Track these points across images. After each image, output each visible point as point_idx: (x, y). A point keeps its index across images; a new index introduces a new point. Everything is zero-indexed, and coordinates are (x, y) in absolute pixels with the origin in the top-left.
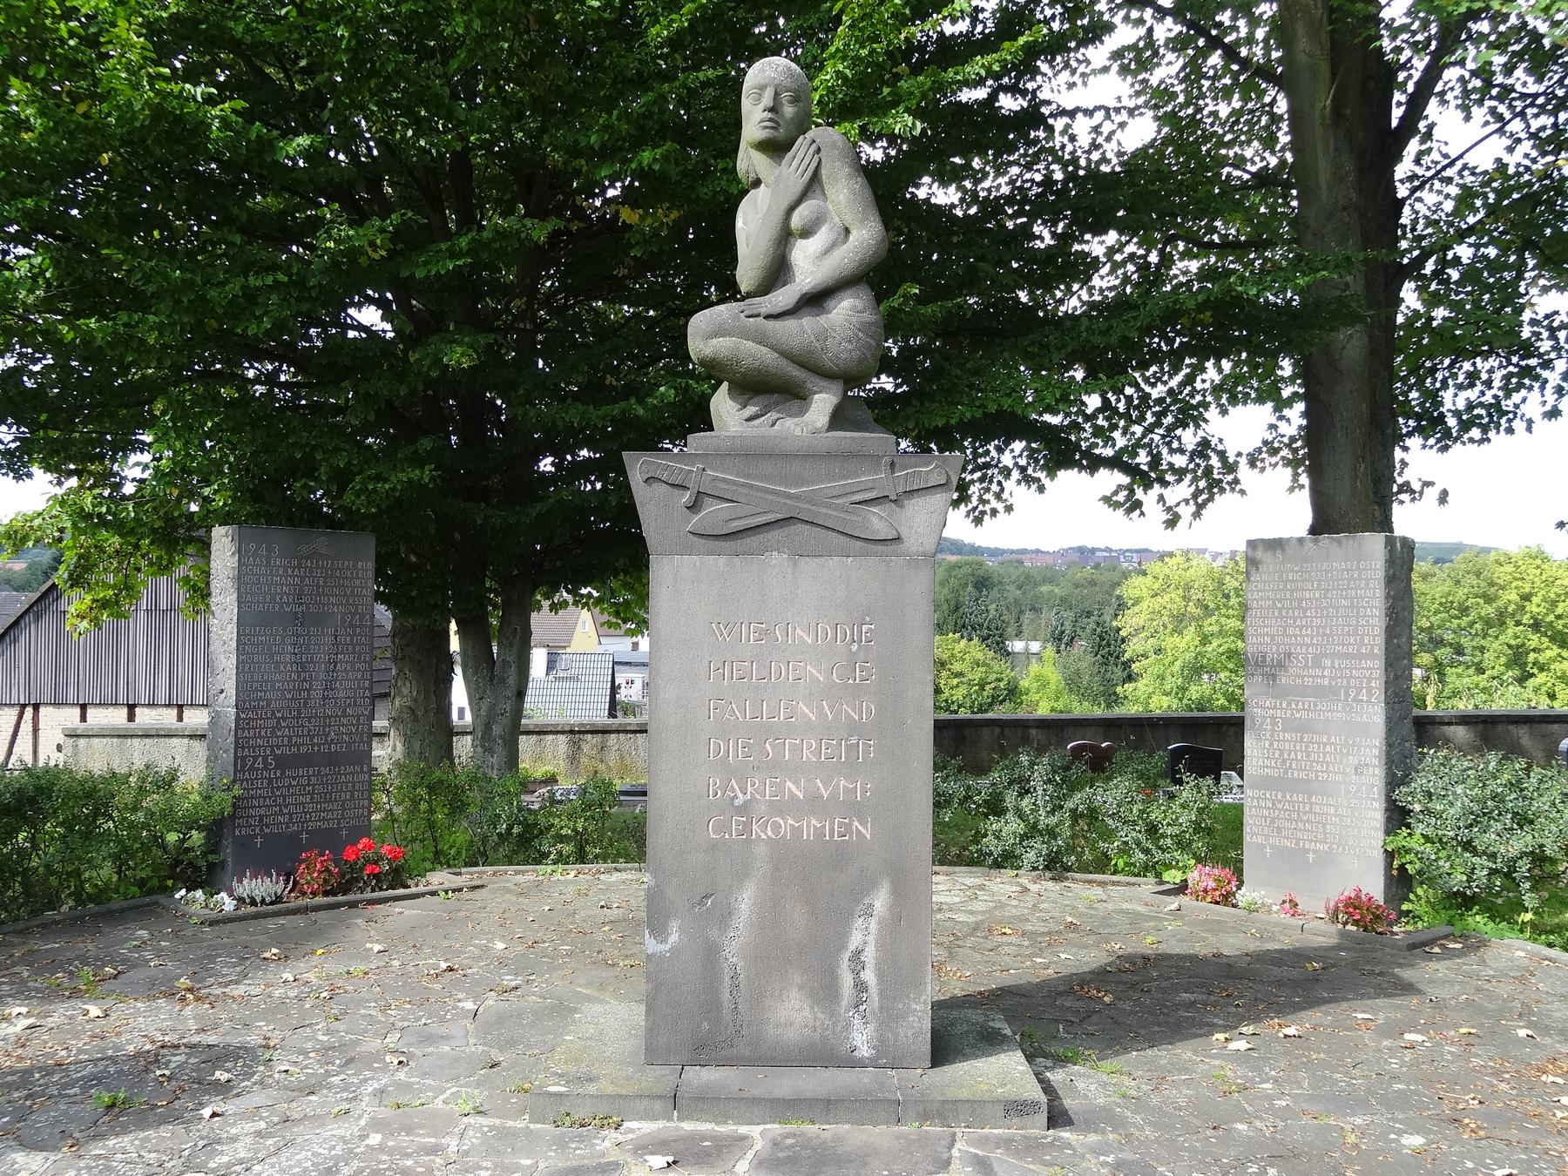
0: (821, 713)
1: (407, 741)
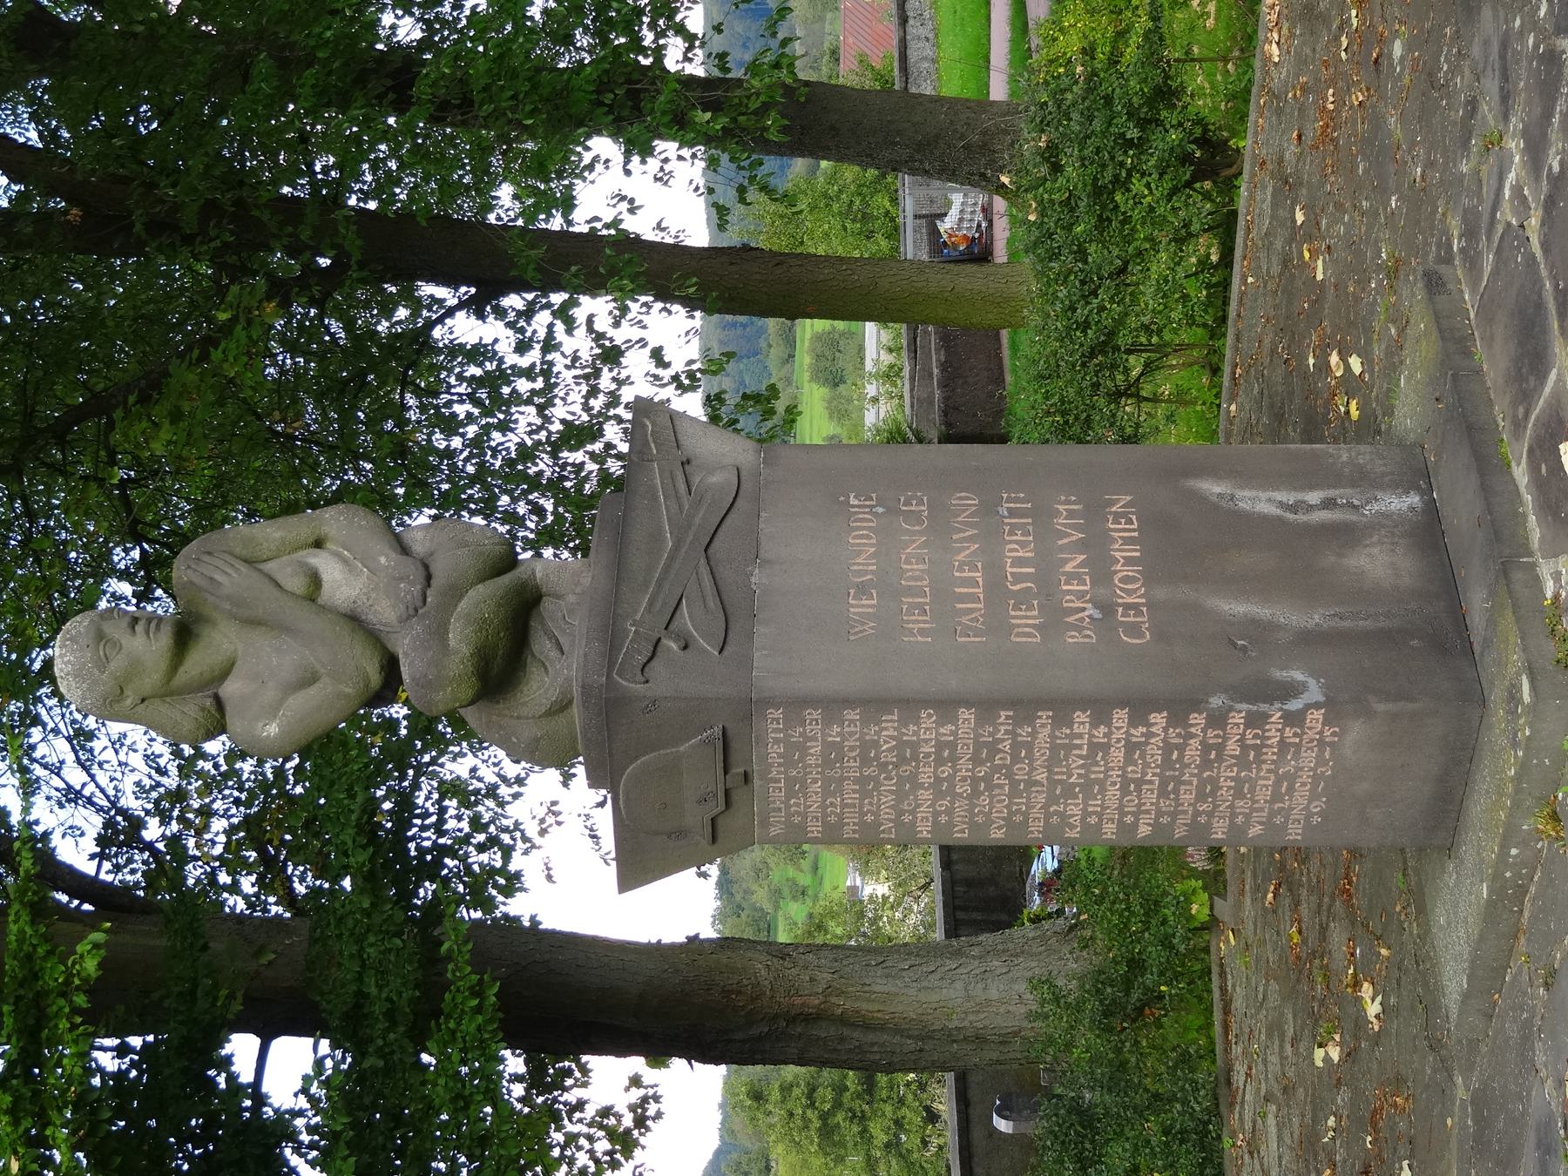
0: (971, 539)
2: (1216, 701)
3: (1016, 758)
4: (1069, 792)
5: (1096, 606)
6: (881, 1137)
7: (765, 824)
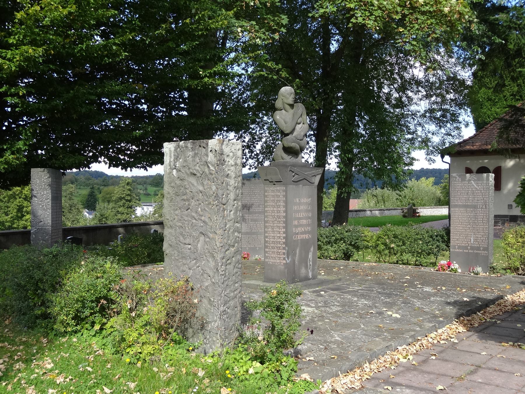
1: (370, 217)
2: (287, 248)
4: (272, 229)
6: (120, 210)
7: (267, 187)
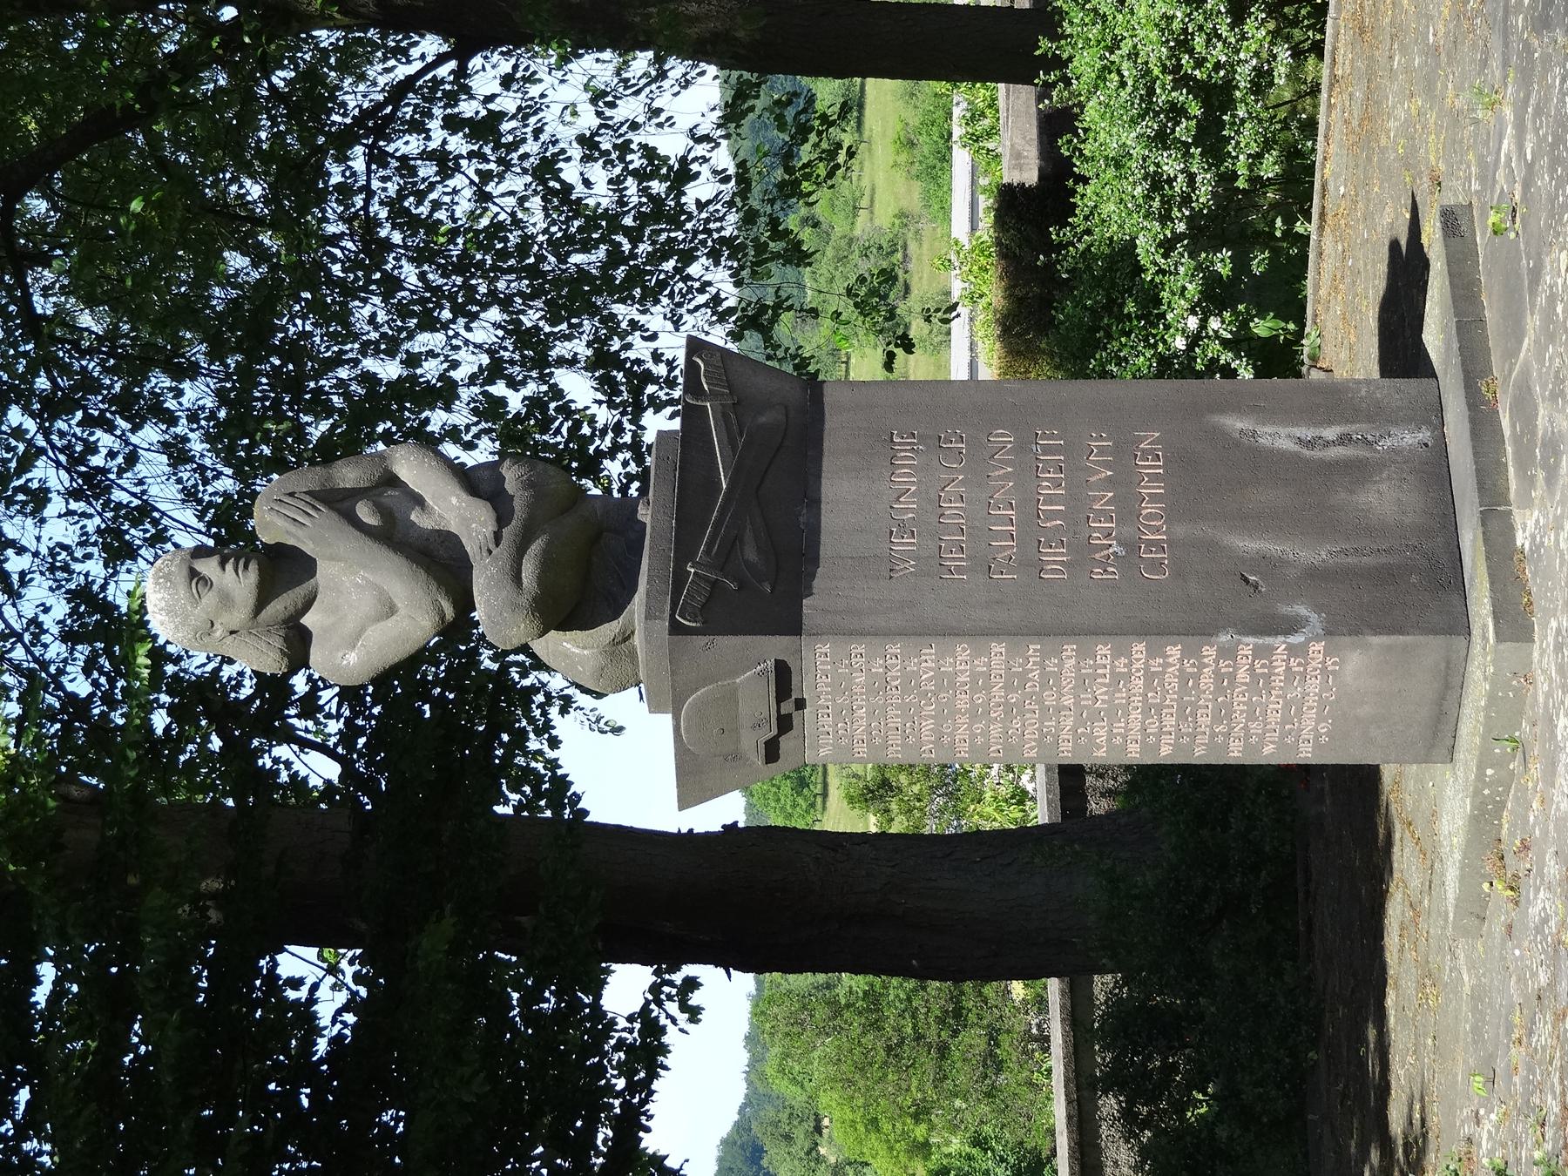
3: (1044, 685)
4: (1096, 716)
5: (1120, 544)
